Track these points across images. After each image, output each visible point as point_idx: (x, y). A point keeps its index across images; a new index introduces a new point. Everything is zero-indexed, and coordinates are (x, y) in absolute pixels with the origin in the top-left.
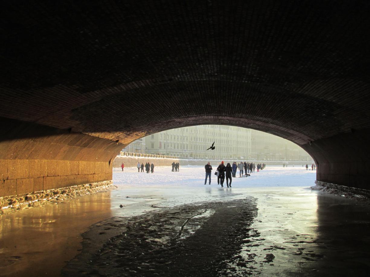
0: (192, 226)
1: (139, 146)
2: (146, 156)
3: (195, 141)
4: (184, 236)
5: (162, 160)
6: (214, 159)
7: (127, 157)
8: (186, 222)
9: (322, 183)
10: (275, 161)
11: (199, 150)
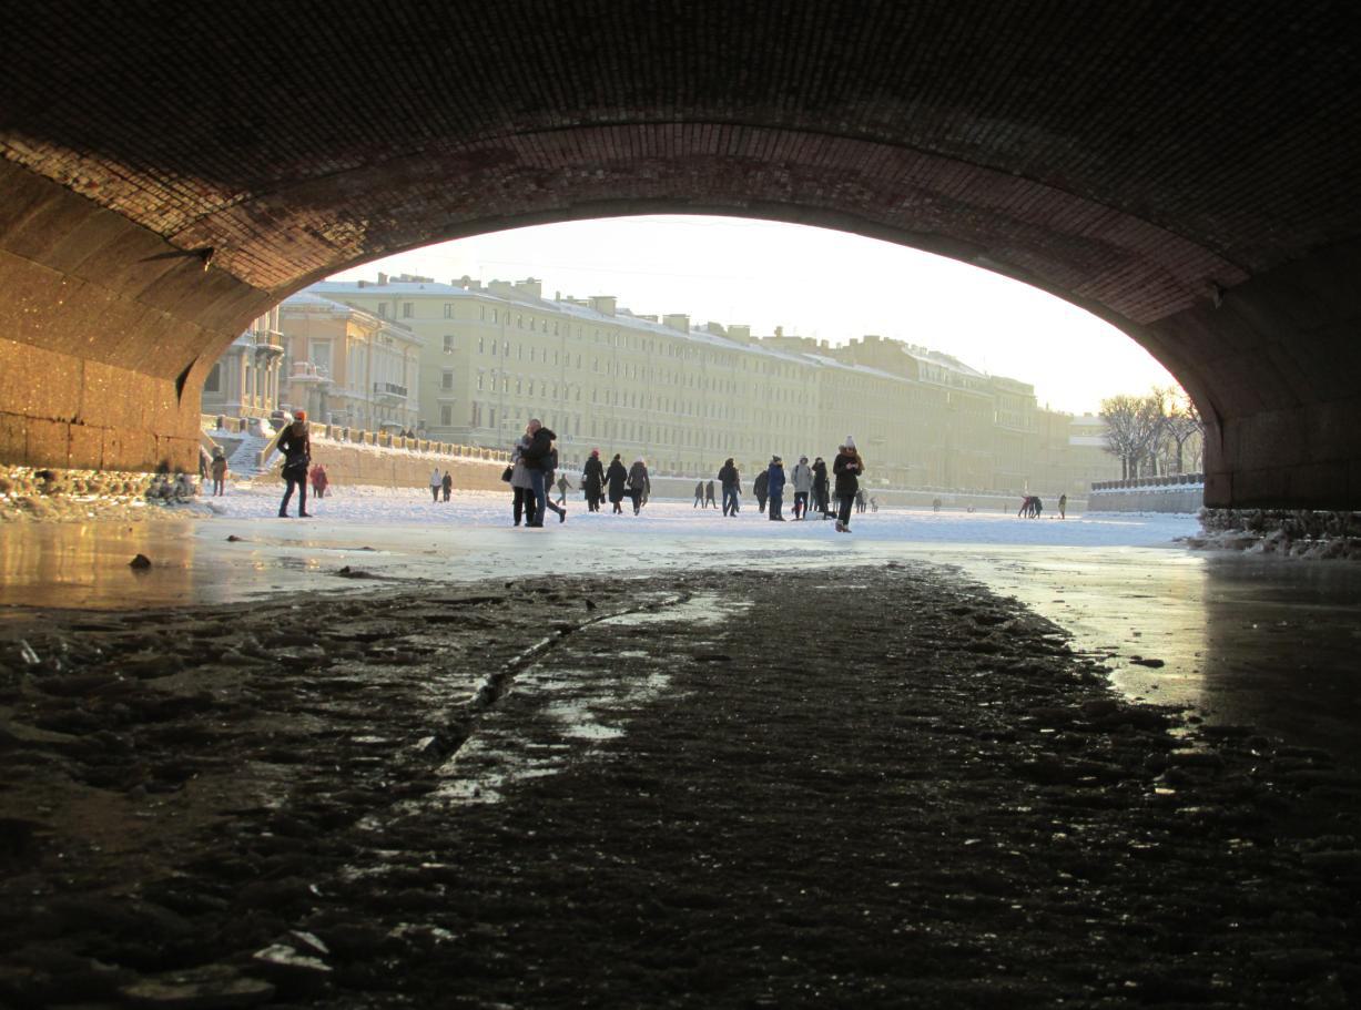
0: (599, 677)
1: (393, 412)
2: (416, 446)
3: (608, 439)
4: (490, 763)
5: (479, 468)
6: (677, 475)
7: (339, 445)
8: (543, 650)
9: (1245, 514)
10: (905, 492)
11: (623, 437)
